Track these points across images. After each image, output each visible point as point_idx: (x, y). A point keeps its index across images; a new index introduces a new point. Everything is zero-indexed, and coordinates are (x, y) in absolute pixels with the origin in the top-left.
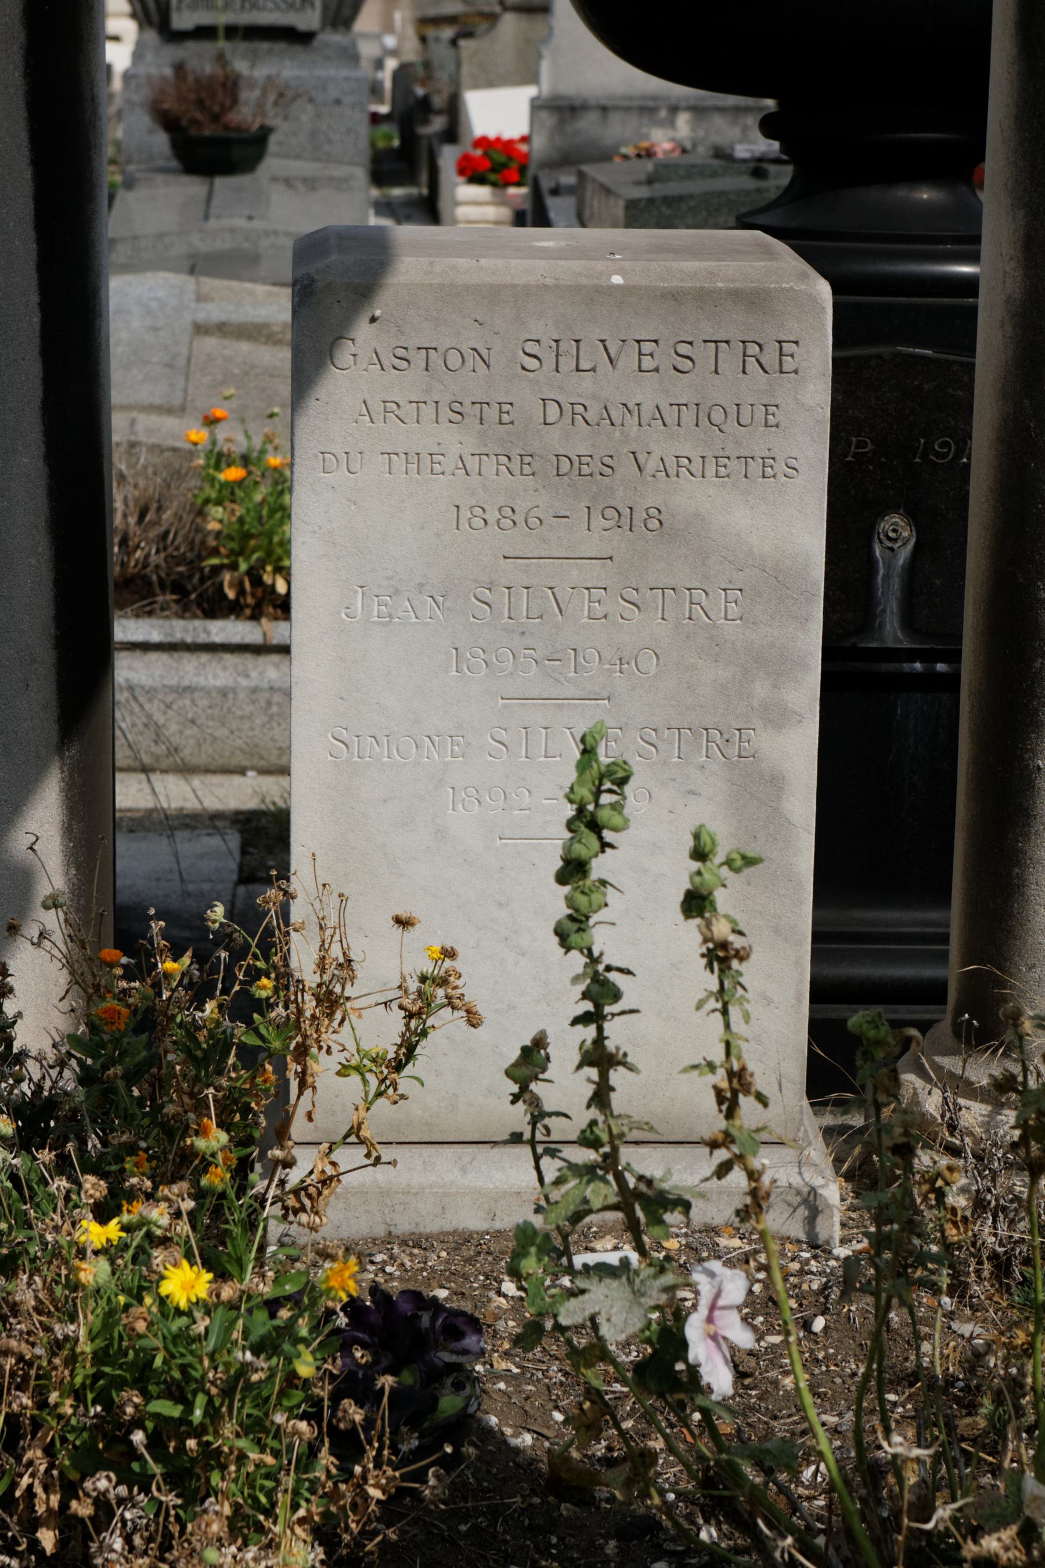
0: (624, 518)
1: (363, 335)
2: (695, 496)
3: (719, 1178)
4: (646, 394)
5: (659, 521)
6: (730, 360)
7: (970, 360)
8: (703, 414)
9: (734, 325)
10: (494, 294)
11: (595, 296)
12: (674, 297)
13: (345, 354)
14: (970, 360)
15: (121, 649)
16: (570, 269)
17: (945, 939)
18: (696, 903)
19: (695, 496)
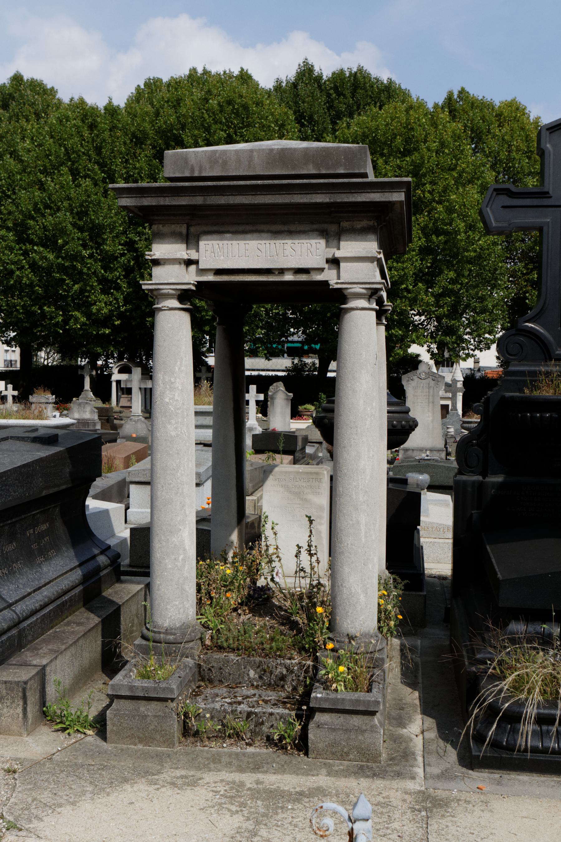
0: (302, 499)
1: (271, 477)
2: (311, 497)
3: (124, 480)
4: (304, 484)
5: (306, 500)
6: (314, 480)
7: (282, 439)
8: (311, 487)
9: (314, 476)
10: (286, 472)
11: (298, 473)
12: (307, 473)
13: (269, 479)
14: (282, 439)
15: (123, 438)
16: (295, 470)
17: (11, 367)
18: (273, 528)
19: (311, 497)
